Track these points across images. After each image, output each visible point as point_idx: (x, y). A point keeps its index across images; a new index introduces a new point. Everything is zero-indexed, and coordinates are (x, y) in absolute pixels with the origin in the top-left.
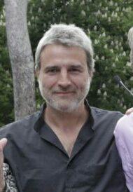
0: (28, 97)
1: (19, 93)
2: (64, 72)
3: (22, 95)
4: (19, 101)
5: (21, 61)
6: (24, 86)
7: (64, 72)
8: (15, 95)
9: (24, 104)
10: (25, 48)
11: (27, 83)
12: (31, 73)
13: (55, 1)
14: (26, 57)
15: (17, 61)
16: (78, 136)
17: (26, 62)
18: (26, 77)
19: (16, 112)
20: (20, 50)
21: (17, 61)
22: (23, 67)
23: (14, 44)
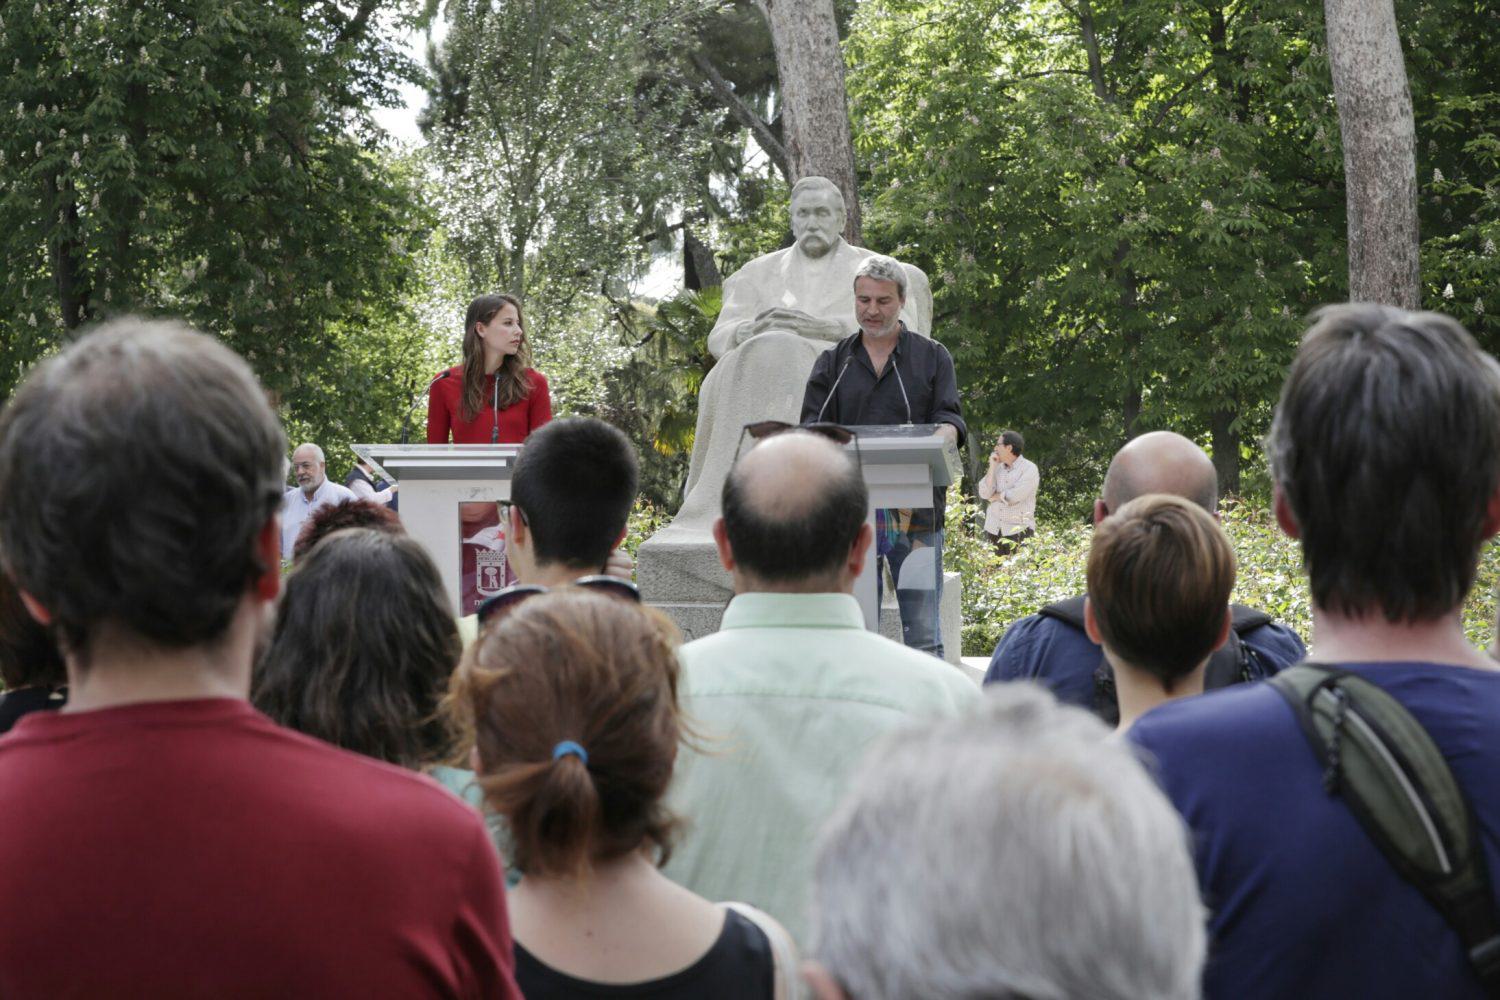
0: (1390, 228)
1: (1361, 213)
2: (873, 303)
3: (1370, 223)
4: (1363, 241)
5: (973, 176)
6: (1379, 195)
7: (873, 303)
8: (1351, 219)
9: (1380, 251)
10: (1382, 74)
11: (1387, 184)
12: (1403, 152)
13: (496, 5)
14: (1387, 100)
15: (1355, 112)
16: (973, 655)
17: (1385, 119)
18: (1384, 162)
19: (1352, 276)
20: (1367, 80)
21: (1355, 112)
22: (1376, 134)
23: (1346, 60)
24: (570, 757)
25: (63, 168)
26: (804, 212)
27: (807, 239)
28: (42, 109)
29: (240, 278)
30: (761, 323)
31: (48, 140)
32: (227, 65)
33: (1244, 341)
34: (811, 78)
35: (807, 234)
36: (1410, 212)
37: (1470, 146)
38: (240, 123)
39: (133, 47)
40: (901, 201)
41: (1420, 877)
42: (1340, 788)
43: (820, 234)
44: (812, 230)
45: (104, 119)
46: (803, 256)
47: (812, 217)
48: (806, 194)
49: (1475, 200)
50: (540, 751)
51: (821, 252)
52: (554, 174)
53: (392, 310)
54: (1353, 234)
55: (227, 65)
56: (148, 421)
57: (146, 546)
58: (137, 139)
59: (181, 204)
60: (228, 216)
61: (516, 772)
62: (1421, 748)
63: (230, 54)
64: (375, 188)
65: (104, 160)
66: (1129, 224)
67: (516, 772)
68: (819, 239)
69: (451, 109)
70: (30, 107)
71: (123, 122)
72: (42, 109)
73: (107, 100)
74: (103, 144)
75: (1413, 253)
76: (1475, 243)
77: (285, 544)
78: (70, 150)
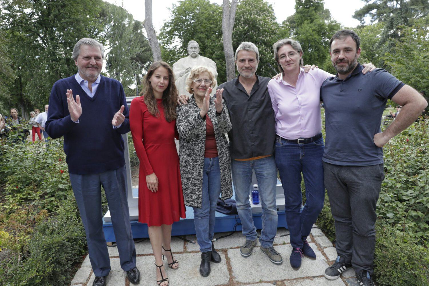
1: (228, 70)
3: (229, 71)
4: (229, 73)
6: (231, 67)
15: (228, 57)
20: (229, 53)
21: (228, 57)
22: (230, 60)
26: (192, 48)
27: (193, 54)
28: (54, 62)
30: (187, 71)
34: (157, 55)
35: (192, 53)
43: (195, 53)
44: (194, 52)
45: (63, 63)
46: (191, 58)
47: (193, 49)
48: (191, 44)
51: (195, 57)
58: (68, 65)
65: (64, 68)
68: (195, 54)
70: (52, 62)
71: (66, 64)
72: (54, 62)
74: (63, 67)
77: (222, 216)
78: (59, 67)
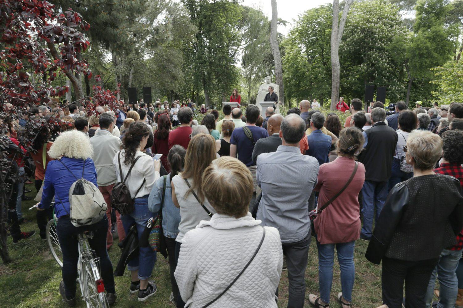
5: (296, 71)
6: (335, 74)
24: (228, 130)
25: (203, 70)
29: (221, 82)
31: (201, 67)
32: (220, 59)
33: (323, 89)
36: (339, 76)
37: (348, 68)
38: (221, 66)
39: (210, 58)
40: (288, 74)
41: (249, 139)
42: (245, 133)
49: (349, 74)
50: (226, 130)
52: (255, 70)
53: (237, 85)
54: (333, 78)
55: (220, 59)
56: (185, 112)
57: (185, 119)
59: (215, 74)
60: (220, 75)
61: (224, 131)
62: (249, 131)
63: (220, 58)
64: (235, 72)
66: (311, 77)
67: (224, 131)
69: (244, 64)
71: (209, 66)
73: (207, 63)
74: (207, 68)
75: (339, 80)
76: (348, 79)
